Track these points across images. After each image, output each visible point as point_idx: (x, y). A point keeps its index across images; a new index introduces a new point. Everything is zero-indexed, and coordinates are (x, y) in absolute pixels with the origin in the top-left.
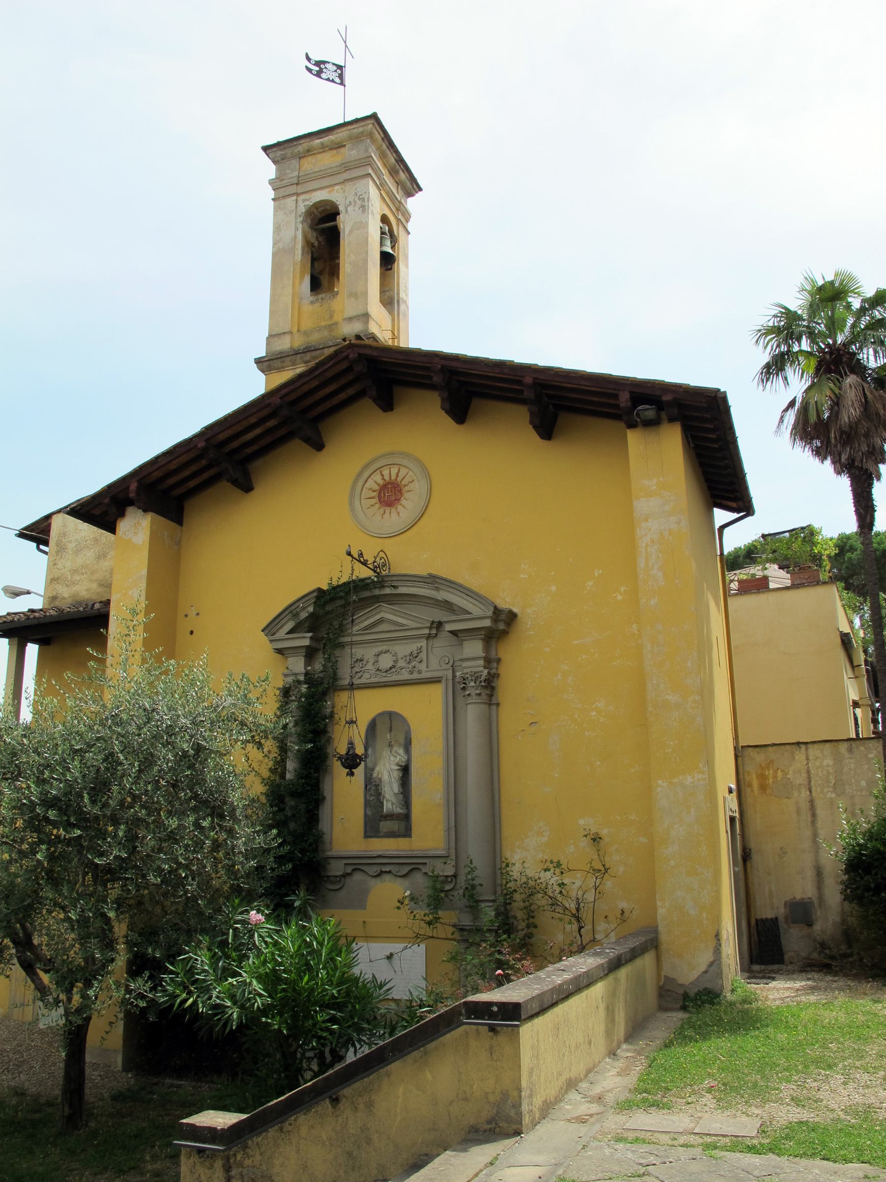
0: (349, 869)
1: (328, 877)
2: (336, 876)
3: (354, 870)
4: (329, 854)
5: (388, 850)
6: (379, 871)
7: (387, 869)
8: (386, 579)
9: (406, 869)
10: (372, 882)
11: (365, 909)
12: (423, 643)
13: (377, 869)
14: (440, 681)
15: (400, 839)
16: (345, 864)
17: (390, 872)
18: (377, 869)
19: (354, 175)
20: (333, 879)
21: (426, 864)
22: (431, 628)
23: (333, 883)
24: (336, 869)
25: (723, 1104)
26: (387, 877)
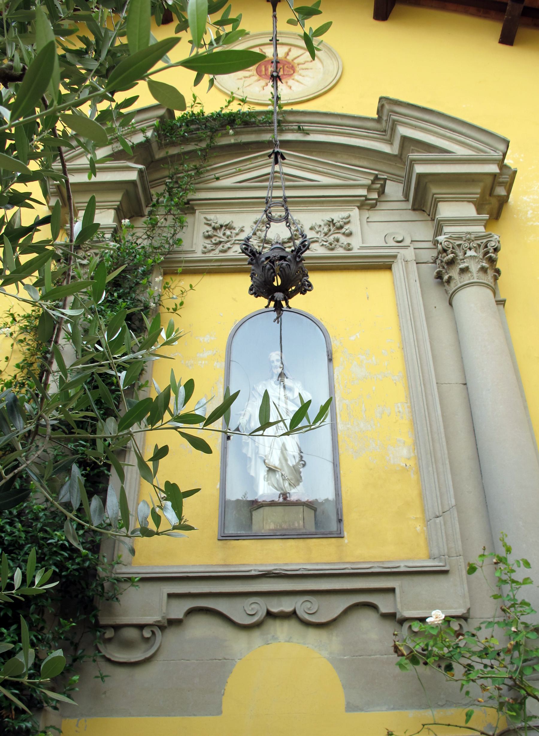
0: (178, 610)
1: (117, 628)
2: (141, 627)
3: (191, 612)
4: (122, 570)
5: (286, 564)
6: (262, 614)
7: (285, 605)
8: (291, 118)
9: (341, 604)
10: (239, 642)
11: (220, 713)
12: (355, 212)
13: (258, 608)
14: (388, 267)
15: (313, 542)
16: (170, 596)
17: (293, 615)
18: (258, 608)
19: (325, 170)
20: (132, 634)
21: (392, 590)
22: (370, 189)
23: (128, 645)
24: (140, 606)
25: (477, 658)
26: (282, 630)
